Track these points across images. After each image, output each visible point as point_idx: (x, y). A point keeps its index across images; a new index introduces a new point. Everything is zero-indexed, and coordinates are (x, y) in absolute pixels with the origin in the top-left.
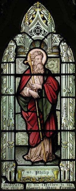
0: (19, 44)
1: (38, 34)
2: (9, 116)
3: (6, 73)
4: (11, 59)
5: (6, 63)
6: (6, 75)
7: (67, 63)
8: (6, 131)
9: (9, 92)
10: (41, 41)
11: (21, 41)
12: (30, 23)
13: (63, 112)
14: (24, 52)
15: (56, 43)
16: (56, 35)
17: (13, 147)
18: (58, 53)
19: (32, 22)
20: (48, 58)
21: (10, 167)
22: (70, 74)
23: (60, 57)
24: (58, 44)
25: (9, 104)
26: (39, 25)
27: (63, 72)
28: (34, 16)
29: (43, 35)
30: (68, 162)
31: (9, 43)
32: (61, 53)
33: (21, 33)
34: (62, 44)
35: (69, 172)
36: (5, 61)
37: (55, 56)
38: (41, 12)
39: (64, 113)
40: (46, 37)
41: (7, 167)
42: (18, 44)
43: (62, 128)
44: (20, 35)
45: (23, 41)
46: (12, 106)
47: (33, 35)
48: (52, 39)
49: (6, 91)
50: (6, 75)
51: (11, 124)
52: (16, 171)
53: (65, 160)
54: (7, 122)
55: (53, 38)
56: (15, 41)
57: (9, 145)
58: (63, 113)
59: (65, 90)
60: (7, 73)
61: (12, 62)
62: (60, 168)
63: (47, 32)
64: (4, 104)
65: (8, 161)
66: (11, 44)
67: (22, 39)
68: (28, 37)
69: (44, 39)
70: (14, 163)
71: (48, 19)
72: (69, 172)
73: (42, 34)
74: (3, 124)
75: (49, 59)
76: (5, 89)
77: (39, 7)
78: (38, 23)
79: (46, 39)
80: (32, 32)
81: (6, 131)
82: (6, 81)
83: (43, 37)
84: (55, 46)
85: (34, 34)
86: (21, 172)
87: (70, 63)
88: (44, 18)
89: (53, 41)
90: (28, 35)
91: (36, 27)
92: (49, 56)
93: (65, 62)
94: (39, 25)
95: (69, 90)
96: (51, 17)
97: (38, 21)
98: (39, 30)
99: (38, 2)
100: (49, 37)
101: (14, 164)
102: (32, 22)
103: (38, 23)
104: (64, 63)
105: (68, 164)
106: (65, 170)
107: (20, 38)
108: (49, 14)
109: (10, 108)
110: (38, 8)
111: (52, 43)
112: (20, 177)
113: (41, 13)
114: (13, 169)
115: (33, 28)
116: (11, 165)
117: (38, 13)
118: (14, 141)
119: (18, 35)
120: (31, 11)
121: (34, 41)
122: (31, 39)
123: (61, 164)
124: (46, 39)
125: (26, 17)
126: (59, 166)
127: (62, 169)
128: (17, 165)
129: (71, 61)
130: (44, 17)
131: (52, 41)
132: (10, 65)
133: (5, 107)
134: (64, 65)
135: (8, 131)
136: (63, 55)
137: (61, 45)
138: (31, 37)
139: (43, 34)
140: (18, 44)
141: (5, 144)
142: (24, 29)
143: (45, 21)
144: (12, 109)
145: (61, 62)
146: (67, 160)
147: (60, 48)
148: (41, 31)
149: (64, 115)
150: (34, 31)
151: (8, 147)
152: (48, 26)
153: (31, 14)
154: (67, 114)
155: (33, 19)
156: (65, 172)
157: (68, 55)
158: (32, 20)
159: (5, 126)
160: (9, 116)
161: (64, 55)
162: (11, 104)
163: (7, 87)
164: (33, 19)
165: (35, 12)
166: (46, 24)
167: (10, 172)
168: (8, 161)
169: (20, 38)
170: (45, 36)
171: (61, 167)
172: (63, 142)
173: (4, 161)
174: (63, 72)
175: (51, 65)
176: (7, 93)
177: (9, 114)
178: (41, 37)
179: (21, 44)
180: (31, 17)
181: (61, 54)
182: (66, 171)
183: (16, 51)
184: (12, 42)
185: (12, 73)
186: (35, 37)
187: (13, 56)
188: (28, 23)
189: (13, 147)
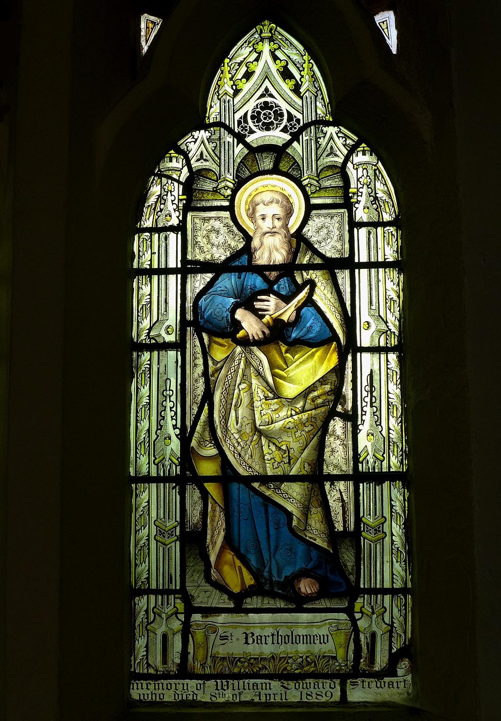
0: (199, 164)
1: (267, 127)
2: (160, 427)
3: (150, 265)
4: (170, 216)
5: (151, 230)
6: (150, 272)
7: (375, 225)
8: (148, 479)
9: (159, 335)
10: (279, 152)
11: (205, 153)
12: (237, 92)
13: (364, 404)
14: (216, 191)
15: (336, 159)
16: (331, 130)
17: (175, 527)
18: (340, 193)
19: (246, 87)
20: (310, 208)
21: (164, 616)
22: (385, 265)
23: (348, 204)
24: (340, 160)
25: (162, 370)
26: (271, 96)
27: (362, 256)
28: (252, 67)
29: (285, 130)
30: (387, 598)
31: (163, 157)
32: (351, 190)
33: (206, 127)
34: (359, 158)
35: (391, 636)
36: (148, 224)
37: (329, 201)
38: (278, 53)
39: (368, 409)
40: (295, 137)
41: (152, 616)
42: (195, 165)
43: (360, 465)
44: (202, 134)
45: (212, 153)
46: (173, 388)
47: (252, 132)
48: (317, 142)
49: (150, 329)
50: (150, 272)
51: (168, 452)
52: (186, 631)
53: (373, 591)
54: (151, 447)
55: (321, 140)
56: (185, 154)
57: (161, 532)
58: (365, 409)
59: (368, 323)
60: (155, 266)
61: (172, 229)
62: (354, 622)
63: (298, 121)
64: (143, 379)
65: (156, 592)
66: (170, 165)
67: (210, 147)
68: (229, 139)
69: (289, 144)
70: (178, 601)
71: (302, 76)
72: (391, 636)
73: (282, 126)
74: (136, 453)
75: (314, 212)
76: (146, 324)
77: (271, 39)
78: (267, 90)
79: (295, 144)
80: (246, 122)
81: (148, 479)
82: (149, 396)
83: (288, 137)
84: (332, 167)
85: (254, 128)
86: (207, 638)
87: (384, 224)
88: (286, 74)
89: (319, 152)
90: (231, 131)
91: (257, 105)
92: (314, 201)
93: (365, 220)
94: (271, 96)
95: (386, 322)
96: (311, 69)
97: (267, 83)
98: (270, 118)
99: (266, 22)
100: (305, 137)
101: (181, 606)
102: (246, 87)
103: (267, 90)
104: (361, 225)
105: (387, 604)
106: (374, 628)
107: (203, 142)
108: (305, 58)
109: (163, 394)
110: (267, 41)
111: (317, 160)
112: (200, 656)
113: (275, 58)
114: (177, 625)
115: (250, 107)
116: (169, 610)
117: (266, 56)
118: (178, 519)
119: (196, 134)
120: (242, 52)
121: (254, 151)
122: (241, 146)
123: (357, 607)
124: (295, 144)
125: (222, 72)
126: (349, 611)
127: (362, 624)
128: (190, 610)
129: (387, 218)
130: (286, 67)
131: (317, 149)
132: (166, 238)
133: (145, 391)
134: (363, 231)
135: (157, 480)
136: (359, 198)
137: (349, 165)
138: (241, 138)
139: (286, 126)
140: (195, 165)
141: (145, 532)
142: (213, 112)
143: (293, 82)
144: (173, 398)
145: (354, 224)
146: (383, 591)
147: (350, 174)
148: (279, 115)
149: (367, 418)
150: (253, 117)
151: (157, 541)
152: (302, 98)
153: (242, 62)
154: (377, 415)
155: (248, 75)
156: (373, 635)
157: (376, 198)
158: (244, 80)
159: (144, 460)
160: (160, 427)
161: (363, 199)
162: (168, 381)
163: (155, 319)
164: (248, 75)
165: (255, 55)
166: (296, 90)
167: (165, 637)
168: (156, 592)
169: (203, 142)
170: (291, 134)
171: (358, 616)
172: (369, 520)
173: (141, 592)
174: (362, 256)
175: (318, 230)
176: (153, 338)
177: (161, 417)
178: (277, 136)
179: (205, 163)
180: (243, 69)
181: (354, 194)
182: (379, 633)
183: (189, 187)
184: (174, 160)
185: (364, 272)
186: (258, 137)
187: (175, 206)
188: (231, 92)
189: (175, 527)
